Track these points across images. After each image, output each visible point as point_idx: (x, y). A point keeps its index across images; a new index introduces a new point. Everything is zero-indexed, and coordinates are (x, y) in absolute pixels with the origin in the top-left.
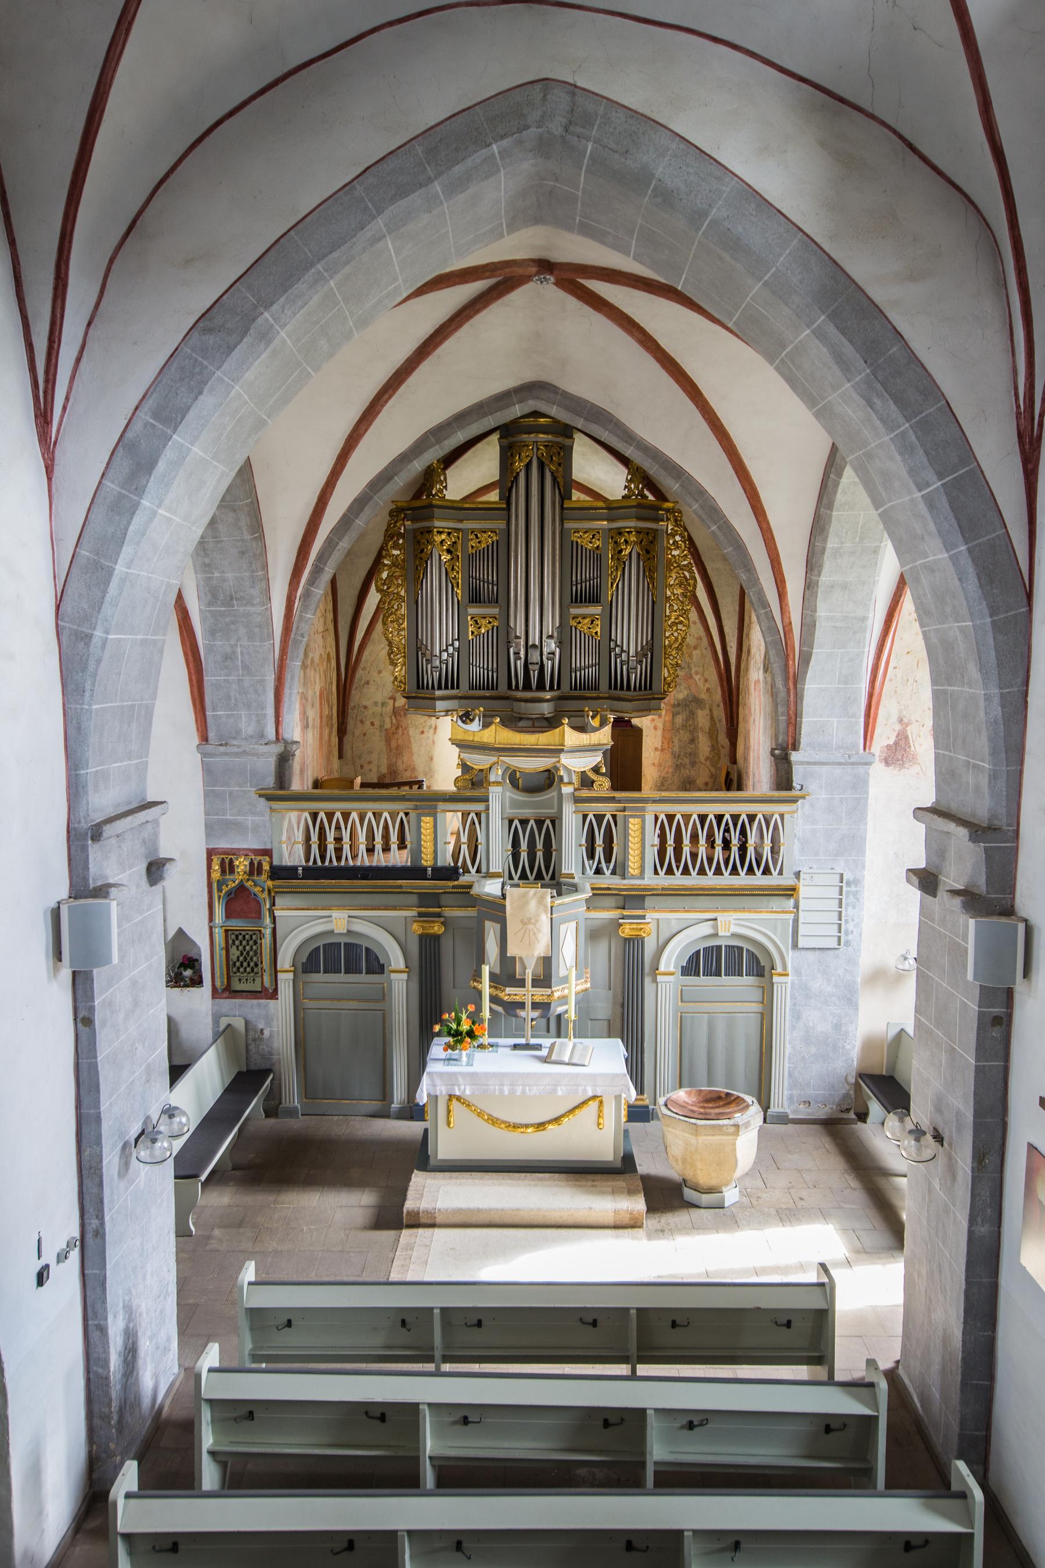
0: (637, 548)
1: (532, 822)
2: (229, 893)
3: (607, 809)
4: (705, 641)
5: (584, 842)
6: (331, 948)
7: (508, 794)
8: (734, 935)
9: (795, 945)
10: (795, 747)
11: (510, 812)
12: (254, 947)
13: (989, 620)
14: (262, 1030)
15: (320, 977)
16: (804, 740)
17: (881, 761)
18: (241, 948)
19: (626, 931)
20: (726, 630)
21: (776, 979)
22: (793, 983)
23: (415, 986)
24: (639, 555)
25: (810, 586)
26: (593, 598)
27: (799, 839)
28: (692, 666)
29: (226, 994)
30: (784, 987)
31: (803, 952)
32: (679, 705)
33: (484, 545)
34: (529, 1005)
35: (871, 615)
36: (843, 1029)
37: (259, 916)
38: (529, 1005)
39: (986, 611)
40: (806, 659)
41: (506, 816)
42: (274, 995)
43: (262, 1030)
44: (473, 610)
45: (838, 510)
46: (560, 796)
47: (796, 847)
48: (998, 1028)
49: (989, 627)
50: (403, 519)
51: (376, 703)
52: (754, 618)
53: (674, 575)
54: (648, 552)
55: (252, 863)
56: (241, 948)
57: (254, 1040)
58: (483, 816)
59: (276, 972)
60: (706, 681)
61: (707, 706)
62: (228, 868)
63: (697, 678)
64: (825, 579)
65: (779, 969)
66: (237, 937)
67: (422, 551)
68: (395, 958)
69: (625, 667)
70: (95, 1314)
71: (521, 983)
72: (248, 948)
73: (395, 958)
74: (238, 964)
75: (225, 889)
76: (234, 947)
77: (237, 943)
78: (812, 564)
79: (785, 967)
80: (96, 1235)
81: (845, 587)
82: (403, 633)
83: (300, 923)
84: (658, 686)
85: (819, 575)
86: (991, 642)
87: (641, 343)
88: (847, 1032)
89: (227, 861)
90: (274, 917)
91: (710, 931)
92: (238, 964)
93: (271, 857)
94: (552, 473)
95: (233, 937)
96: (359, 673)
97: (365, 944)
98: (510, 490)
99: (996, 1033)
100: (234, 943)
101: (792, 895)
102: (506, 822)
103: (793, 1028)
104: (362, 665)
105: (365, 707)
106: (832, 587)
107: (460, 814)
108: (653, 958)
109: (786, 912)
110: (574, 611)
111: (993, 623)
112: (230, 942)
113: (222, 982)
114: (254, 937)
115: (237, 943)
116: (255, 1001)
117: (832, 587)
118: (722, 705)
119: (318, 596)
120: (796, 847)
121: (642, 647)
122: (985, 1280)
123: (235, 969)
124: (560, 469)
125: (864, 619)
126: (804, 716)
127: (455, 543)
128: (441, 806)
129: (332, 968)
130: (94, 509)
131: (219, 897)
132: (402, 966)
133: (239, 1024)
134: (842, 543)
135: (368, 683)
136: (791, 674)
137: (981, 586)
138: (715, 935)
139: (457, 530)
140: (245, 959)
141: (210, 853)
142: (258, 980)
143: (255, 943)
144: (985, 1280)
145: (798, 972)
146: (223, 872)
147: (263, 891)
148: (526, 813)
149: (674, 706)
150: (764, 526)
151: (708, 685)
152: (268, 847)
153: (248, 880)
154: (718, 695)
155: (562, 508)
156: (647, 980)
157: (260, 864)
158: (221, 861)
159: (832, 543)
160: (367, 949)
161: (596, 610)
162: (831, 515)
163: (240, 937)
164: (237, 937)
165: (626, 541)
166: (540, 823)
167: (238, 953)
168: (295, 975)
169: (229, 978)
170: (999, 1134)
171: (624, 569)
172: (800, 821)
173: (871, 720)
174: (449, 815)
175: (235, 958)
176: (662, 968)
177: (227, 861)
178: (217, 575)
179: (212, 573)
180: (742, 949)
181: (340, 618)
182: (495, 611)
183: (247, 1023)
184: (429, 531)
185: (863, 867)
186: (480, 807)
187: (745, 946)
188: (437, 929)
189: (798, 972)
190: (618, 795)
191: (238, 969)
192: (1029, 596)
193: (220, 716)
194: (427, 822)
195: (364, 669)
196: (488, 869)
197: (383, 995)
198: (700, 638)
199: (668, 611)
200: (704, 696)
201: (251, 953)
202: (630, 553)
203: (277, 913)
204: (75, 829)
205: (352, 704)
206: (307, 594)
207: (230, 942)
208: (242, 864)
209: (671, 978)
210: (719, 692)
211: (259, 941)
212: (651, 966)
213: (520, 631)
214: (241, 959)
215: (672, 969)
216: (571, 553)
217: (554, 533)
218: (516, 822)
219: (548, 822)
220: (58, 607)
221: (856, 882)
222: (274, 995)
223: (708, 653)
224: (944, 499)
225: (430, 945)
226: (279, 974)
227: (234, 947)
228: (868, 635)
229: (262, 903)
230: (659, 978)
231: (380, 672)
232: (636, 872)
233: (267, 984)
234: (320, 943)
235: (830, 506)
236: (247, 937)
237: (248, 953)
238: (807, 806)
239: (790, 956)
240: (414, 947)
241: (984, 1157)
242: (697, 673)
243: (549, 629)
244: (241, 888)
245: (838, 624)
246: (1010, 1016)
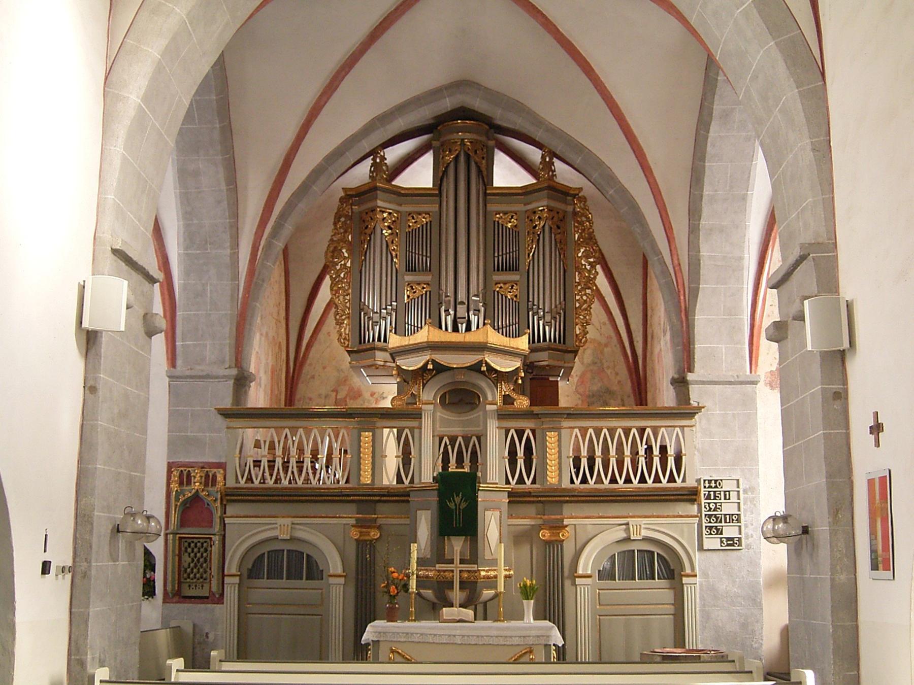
0: (549, 222)
1: (460, 439)
2: (185, 502)
3: (527, 425)
4: (615, 340)
5: (506, 454)
6: (275, 555)
7: (439, 414)
8: (646, 539)
9: (701, 548)
10: (690, 369)
11: (441, 430)
12: (205, 555)
13: (808, 141)
14: (207, 634)
15: (264, 582)
16: (697, 366)
17: (766, 384)
18: (192, 555)
19: (545, 535)
20: (633, 327)
21: (685, 580)
22: (701, 585)
23: (351, 590)
24: (551, 228)
25: (694, 230)
26: (513, 268)
27: (698, 451)
28: (604, 361)
29: (176, 599)
30: (694, 589)
31: (708, 553)
32: (593, 395)
33: (417, 295)
34: (457, 585)
35: (746, 256)
36: (750, 628)
37: (210, 524)
38: (457, 585)
39: (794, 85)
40: (694, 293)
41: (436, 434)
42: (219, 599)
43: (207, 634)
44: (408, 278)
45: (709, 162)
46: (485, 411)
47: (697, 458)
48: (838, 402)
49: (809, 147)
50: (352, 205)
51: (320, 395)
52: (653, 276)
53: (582, 250)
54: (558, 227)
55: (207, 476)
56: (192, 555)
57: (199, 643)
58: (416, 431)
59: (223, 576)
60: (617, 374)
61: (619, 398)
62: (185, 479)
63: (609, 372)
64: (705, 223)
65: (688, 571)
66: (189, 544)
67: (367, 227)
68: (334, 563)
69: (541, 322)
70: (78, 650)
71: (451, 562)
72: (199, 555)
73: (334, 563)
74: (189, 570)
75: (182, 498)
76: (187, 554)
77: (189, 550)
78: (694, 213)
79: (693, 568)
80: (84, 577)
81: (721, 230)
82: (348, 298)
83: (247, 531)
84: (570, 343)
85: (699, 220)
86: (800, 107)
87: (543, 25)
88: (753, 631)
89: (185, 473)
90: (225, 525)
91: (623, 535)
92: (189, 570)
93: (225, 470)
94: (476, 163)
95: (186, 544)
96: (306, 369)
97: (306, 550)
98: (442, 180)
99: (837, 405)
100: (186, 551)
101: (695, 500)
102: (437, 440)
103: (704, 628)
104: (308, 362)
105: (310, 399)
106: (711, 230)
107: (395, 430)
108: (572, 561)
109: (692, 517)
110: (496, 277)
111: (799, 92)
112: (183, 549)
113: (173, 586)
114: (205, 545)
115: (189, 550)
116: (203, 606)
117: (711, 230)
118: (632, 396)
119: (278, 249)
120: (697, 458)
121: (556, 307)
122: (848, 623)
123: (185, 575)
124: (484, 162)
125: (741, 258)
126: (696, 343)
127: (394, 221)
128: (380, 423)
129: (274, 574)
130: (140, 13)
131: (176, 505)
132: (340, 571)
133: (188, 628)
134: (716, 191)
135: (313, 377)
136: (683, 307)
137: (788, 68)
138: (628, 539)
139: (397, 212)
140: (196, 566)
141: (170, 466)
142: (206, 586)
143: (206, 550)
144: (848, 623)
145: (705, 575)
146: (181, 483)
147: (216, 500)
148: (456, 430)
149: (589, 396)
150: (651, 181)
151: (618, 378)
152: (223, 460)
153: (203, 490)
154: (628, 387)
155: (485, 194)
156: (567, 583)
157: (214, 476)
158: (180, 473)
159: (707, 191)
160: (308, 556)
161: (515, 277)
162: (704, 167)
163: (192, 545)
164: (189, 544)
165: (539, 218)
166: (467, 439)
167: (190, 560)
168: (240, 580)
169: (180, 583)
170: (848, 491)
171: (539, 240)
172: (699, 435)
173: (754, 348)
174: (386, 431)
175: (186, 565)
176: (580, 571)
177: (185, 473)
178: (195, 221)
179: (192, 220)
180: (653, 553)
181: (291, 317)
182: (428, 278)
183: (194, 626)
184: (373, 210)
185: (758, 475)
186: (414, 423)
187: (656, 550)
188: (374, 534)
189: (705, 575)
190: (536, 409)
191: (189, 575)
192: (823, 74)
193: (188, 346)
194: (367, 436)
195: (311, 365)
196: (420, 480)
197: (324, 601)
198: (609, 337)
199: (577, 278)
200: (615, 388)
201: (202, 560)
202: (544, 226)
203: (227, 521)
204: (100, 238)
205: (298, 397)
206: (269, 245)
207: (183, 549)
208: (197, 475)
209: (588, 581)
210: (629, 384)
211: (209, 549)
212: (571, 566)
213: (451, 293)
214: (192, 565)
215: (589, 572)
216: (494, 233)
217: (478, 214)
218: (446, 439)
219: (474, 438)
220: (106, 78)
221: (752, 489)
222: (219, 599)
223: (618, 350)
224: (755, 11)
225: (365, 548)
226: (226, 578)
227: (187, 554)
228: (745, 274)
229: (214, 511)
230: (578, 581)
231: (324, 368)
232: (556, 473)
233: (214, 589)
234: (265, 549)
235: (703, 159)
236: (199, 544)
237: (198, 560)
238: (704, 422)
239: (697, 557)
240: (351, 550)
241: (837, 511)
242: (608, 368)
243: (473, 290)
244: (196, 497)
245: (719, 263)
246: (846, 391)
